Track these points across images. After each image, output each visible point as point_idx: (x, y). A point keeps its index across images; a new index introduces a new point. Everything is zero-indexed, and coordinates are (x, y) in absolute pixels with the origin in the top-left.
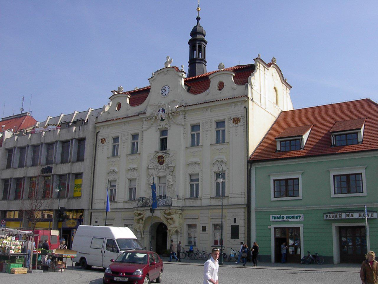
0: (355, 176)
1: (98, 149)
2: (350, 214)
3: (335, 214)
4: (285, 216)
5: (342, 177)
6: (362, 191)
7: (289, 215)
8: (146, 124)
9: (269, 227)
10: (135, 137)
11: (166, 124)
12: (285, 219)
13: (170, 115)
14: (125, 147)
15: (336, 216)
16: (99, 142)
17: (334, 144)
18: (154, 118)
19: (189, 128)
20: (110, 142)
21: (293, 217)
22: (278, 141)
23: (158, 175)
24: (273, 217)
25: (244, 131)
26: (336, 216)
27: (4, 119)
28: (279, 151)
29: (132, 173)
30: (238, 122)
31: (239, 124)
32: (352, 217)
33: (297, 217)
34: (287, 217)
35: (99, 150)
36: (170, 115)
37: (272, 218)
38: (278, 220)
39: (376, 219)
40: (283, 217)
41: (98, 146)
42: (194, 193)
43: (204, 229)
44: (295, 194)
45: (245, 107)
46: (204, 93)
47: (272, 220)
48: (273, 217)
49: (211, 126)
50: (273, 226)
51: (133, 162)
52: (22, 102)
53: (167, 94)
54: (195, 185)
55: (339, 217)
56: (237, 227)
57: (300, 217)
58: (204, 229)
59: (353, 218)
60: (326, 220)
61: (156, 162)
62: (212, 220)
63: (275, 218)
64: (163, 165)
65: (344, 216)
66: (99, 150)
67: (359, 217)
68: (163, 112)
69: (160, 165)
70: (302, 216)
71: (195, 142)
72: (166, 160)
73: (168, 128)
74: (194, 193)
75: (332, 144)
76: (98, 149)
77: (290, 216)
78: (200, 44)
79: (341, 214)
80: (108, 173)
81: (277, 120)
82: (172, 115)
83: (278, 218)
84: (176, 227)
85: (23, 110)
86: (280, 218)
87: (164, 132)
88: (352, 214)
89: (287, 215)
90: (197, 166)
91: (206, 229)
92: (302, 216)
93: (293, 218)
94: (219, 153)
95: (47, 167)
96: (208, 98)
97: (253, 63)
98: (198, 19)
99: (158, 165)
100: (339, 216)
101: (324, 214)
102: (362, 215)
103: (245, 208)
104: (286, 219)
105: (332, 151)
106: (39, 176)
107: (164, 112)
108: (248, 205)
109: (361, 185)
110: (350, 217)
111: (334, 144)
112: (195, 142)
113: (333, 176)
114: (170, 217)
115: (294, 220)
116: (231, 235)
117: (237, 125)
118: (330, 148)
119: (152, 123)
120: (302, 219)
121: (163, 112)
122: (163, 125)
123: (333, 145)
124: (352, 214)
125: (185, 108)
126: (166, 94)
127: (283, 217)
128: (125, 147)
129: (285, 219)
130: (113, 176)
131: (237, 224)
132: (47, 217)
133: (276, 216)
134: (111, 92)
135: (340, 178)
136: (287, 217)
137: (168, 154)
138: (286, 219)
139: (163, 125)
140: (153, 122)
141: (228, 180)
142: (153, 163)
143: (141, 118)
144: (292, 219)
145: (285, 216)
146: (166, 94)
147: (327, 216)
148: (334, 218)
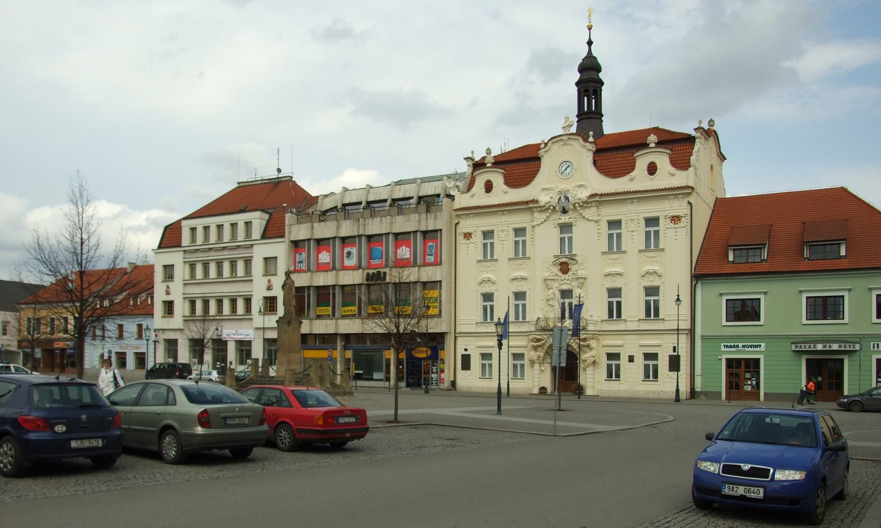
0: (835, 299)
1: (460, 250)
2: (828, 344)
3: (808, 344)
4: (740, 345)
5: (816, 299)
6: (841, 318)
7: (746, 344)
8: (539, 217)
9: (719, 357)
10: (519, 232)
11: (569, 218)
12: (740, 348)
13: (577, 205)
14: (504, 246)
15: (801, 347)
16: (460, 238)
17: (808, 256)
18: (551, 208)
19: (605, 226)
20: (478, 239)
21: (751, 346)
22: (732, 249)
23: (560, 288)
24: (724, 346)
25: (687, 233)
26: (810, 347)
27: (242, 185)
28: (733, 262)
29: (519, 284)
30: (679, 222)
31: (681, 224)
32: (830, 349)
33: (756, 346)
34: (743, 346)
35: (461, 249)
36: (577, 205)
37: (723, 346)
38: (754, 349)
39: (858, 351)
40: (738, 346)
41: (459, 243)
42: (615, 311)
43: (631, 359)
44: (820, 301)
45: (689, 203)
46: (627, 177)
47: (723, 349)
48: (724, 346)
49: (639, 225)
50: (724, 357)
51: (519, 268)
52: (277, 158)
53: (569, 173)
54: (520, 305)
55: (814, 348)
56: (678, 357)
57: (760, 346)
58: (631, 359)
59: (831, 349)
60: (793, 351)
61: (556, 270)
62: (642, 348)
63: (727, 346)
64: (567, 275)
65: (820, 347)
66: (461, 249)
67: (824, 349)
68: (567, 201)
69: (564, 274)
70: (763, 345)
71: (614, 244)
72: (573, 268)
73: (574, 224)
74: (615, 311)
75: (805, 257)
76: (460, 248)
77: (747, 345)
78: (595, 88)
79: (816, 344)
80: (480, 283)
81: (713, 212)
82: (580, 206)
83: (731, 347)
84: (594, 357)
85: (279, 170)
86: (734, 346)
87: (566, 228)
88: (830, 345)
89: (743, 344)
90: (619, 277)
91: (635, 359)
92: (763, 345)
93: (751, 348)
94: (651, 261)
95: (376, 272)
96: (633, 187)
97: (693, 133)
98: (590, 43)
99: (560, 273)
100: (813, 347)
101: (792, 343)
102: (843, 346)
103: (687, 334)
104: (741, 348)
105: (807, 266)
106: (361, 284)
107: (569, 201)
108: (692, 332)
109: (841, 310)
110: (827, 349)
111: (808, 256)
112: (614, 244)
113: (875, 296)
114: (585, 344)
115: (753, 349)
116: (669, 367)
117: (676, 226)
118: (802, 262)
119: (548, 215)
120: (763, 348)
121: (567, 201)
122: (565, 219)
123: (807, 258)
124: (830, 345)
125: (598, 199)
126: (567, 174)
127: (738, 346)
128: (504, 246)
129: (740, 348)
130: (489, 287)
131: (165, 284)
132: (196, 358)
133: (729, 344)
134: (464, 159)
135: (815, 300)
136: (743, 346)
137: (576, 260)
138: (741, 348)
139: (565, 219)
140: (549, 213)
141: (663, 298)
142: (551, 272)
143: (531, 208)
144: (750, 348)
145: (740, 345)
146: (567, 174)
147: (797, 346)
148: (806, 349)
